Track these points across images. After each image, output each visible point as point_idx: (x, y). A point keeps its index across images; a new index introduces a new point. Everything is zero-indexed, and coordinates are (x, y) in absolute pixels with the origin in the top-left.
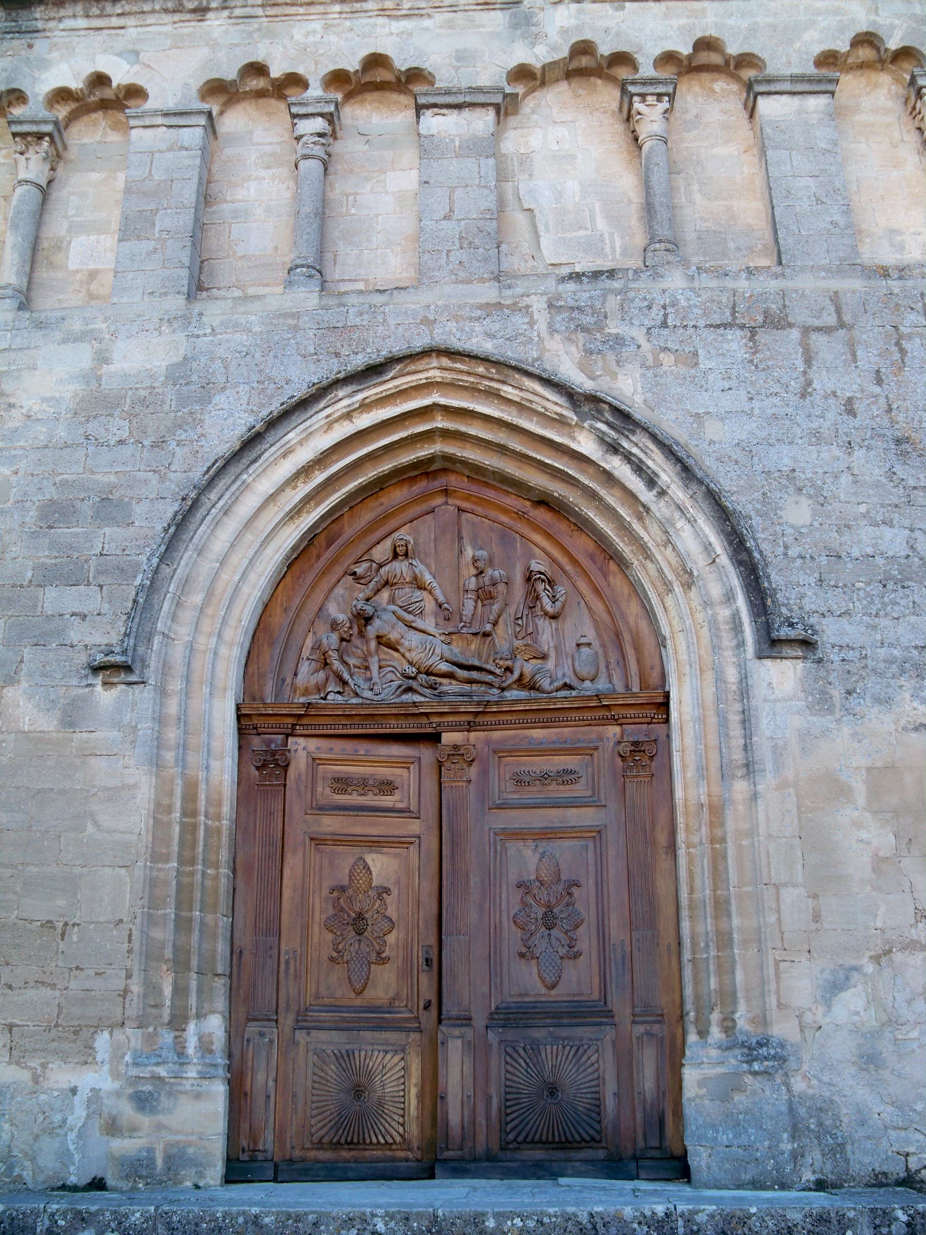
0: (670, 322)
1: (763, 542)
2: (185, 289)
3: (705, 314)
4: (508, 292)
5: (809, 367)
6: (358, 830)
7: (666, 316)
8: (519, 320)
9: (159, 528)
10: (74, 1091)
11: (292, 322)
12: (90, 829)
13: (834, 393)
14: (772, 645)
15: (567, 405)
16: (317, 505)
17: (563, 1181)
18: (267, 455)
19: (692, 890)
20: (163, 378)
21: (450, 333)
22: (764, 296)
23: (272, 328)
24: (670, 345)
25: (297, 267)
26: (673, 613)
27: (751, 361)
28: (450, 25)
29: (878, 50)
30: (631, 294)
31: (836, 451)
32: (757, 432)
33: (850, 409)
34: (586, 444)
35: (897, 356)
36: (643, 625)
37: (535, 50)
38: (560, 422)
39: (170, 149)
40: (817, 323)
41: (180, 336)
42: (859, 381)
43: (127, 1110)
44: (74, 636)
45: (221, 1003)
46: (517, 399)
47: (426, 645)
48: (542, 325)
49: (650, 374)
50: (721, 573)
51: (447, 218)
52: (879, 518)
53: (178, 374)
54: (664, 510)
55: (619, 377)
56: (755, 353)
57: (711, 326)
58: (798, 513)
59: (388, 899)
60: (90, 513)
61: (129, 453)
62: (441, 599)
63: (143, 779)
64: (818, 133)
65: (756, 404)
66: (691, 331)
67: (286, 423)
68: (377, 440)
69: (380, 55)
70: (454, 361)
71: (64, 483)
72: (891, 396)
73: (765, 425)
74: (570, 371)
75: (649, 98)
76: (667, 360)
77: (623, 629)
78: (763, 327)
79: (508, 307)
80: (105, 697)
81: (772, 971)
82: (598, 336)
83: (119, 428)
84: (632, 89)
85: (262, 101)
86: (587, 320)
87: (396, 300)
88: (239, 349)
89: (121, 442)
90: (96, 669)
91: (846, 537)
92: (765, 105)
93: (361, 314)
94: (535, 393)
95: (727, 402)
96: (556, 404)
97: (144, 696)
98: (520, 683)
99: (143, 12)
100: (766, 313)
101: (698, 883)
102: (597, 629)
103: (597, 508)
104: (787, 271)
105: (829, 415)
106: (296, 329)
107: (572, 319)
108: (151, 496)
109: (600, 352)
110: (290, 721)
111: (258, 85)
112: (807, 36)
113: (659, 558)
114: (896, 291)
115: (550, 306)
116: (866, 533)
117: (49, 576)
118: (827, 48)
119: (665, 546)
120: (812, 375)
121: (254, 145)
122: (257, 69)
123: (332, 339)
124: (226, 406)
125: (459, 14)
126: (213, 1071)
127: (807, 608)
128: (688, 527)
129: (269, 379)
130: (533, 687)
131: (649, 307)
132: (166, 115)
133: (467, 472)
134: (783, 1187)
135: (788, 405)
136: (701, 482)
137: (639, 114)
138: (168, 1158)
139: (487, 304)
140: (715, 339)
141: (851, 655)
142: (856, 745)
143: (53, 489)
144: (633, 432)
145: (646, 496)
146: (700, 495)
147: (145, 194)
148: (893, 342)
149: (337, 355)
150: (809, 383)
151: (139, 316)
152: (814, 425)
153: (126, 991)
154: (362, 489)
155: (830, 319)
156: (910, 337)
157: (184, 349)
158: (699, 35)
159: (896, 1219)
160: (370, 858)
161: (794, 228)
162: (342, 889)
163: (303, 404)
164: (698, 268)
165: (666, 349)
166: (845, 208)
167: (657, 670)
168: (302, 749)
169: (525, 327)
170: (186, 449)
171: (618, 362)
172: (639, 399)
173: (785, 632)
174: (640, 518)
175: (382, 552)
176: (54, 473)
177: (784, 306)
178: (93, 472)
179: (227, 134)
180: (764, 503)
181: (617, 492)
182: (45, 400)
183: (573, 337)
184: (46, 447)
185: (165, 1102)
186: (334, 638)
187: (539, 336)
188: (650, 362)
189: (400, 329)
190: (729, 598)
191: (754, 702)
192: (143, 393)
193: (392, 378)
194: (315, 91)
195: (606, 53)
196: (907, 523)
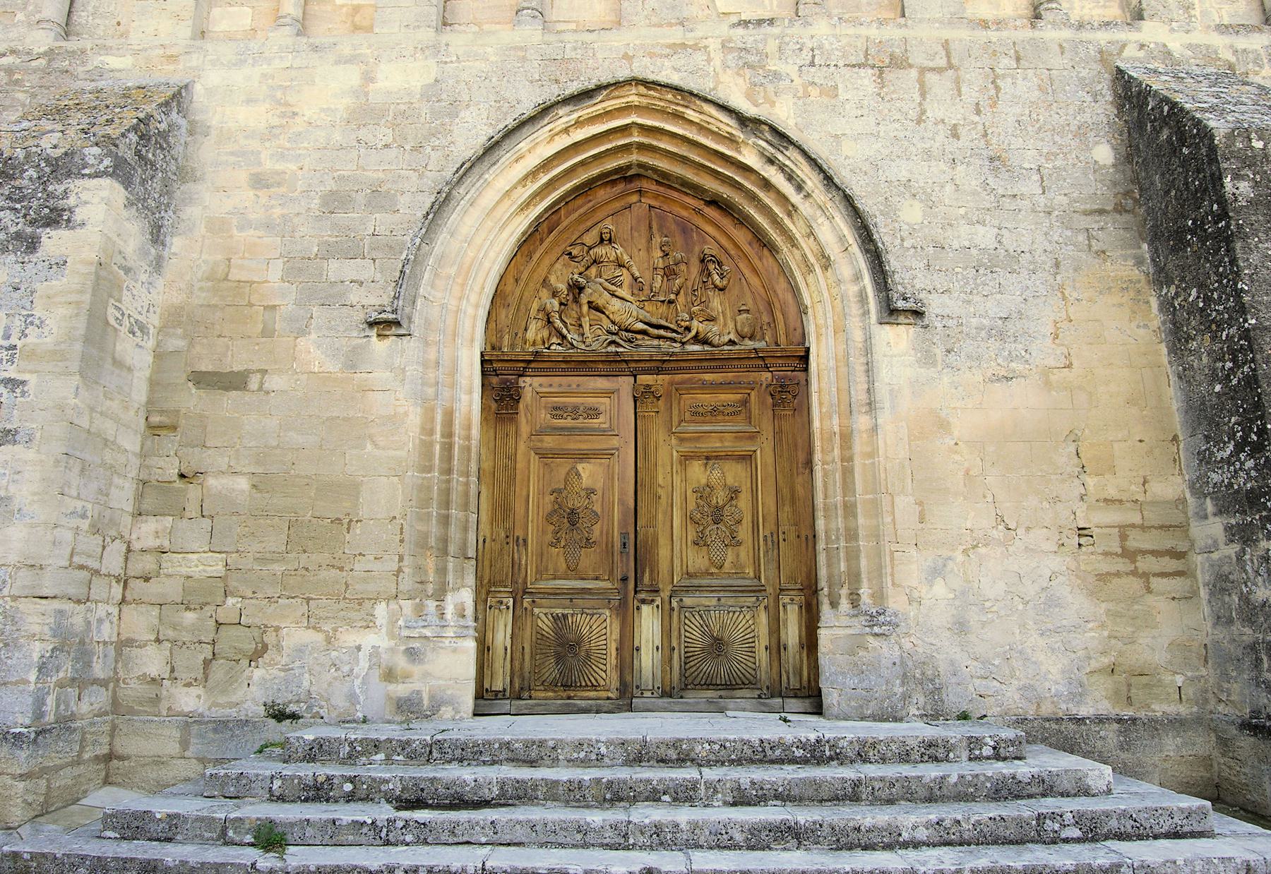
0: (817, 61)
1: (883, 234)
2: (434, 24)
4: (692, 35)
6: (572, 446)
7: (813, 56)
8: (699, 57)
9: (420, 214)
10: (359, 648)
11: (521, 54)
12: (369, 447)
13: (943, 120)
14: (891, 313)
16: (542, 200)
17: (729, 713)
18: (503, 159)
19: (826, 497)
21: (646, 67)
24: (816, 80)
25: (524, 9)
26: (813, 288)
30: (787, 39)
31: (942, 166)
34: (750, 158)
35: (993, 92)
36: (789, 297)
40: (931, 64)
41: (432, 62)
42: (962, 111)
43: (401, 662)
44: (353, 298)
45: (471, 579)
47: (624, 310)
48: (717, 62)
49: (800, 103)
50: (852, 259)
52: (975, 219)
53: (432, 91)
54: (809, 209)
58: (911, 213)
59: (594, 497)
60: (364, 202)
62: (637, 274)
63: (411, 409)
66: (832, 69)
67: (518, 134)
68: (587, 151)
70: (649, 89)
71: (341, 178)
76: (814, 92)
77: (775, 300)
80: (380, 346)
81: (888, 559)
82: (761, 71)
83: (384, 134)
86: (752, 59)
89: (386, 146)
90: (372, 324)
91: (949, 233)
98: (697, 339)
101: (830, 492)
102: (754, 299)
103: (756, 206)
104: (910, 22)
105: (938, 138)
106: (524, 59)
109: (762, 85)
110: (522, 365)
113: (804, 246)
114: (994, 40)
116: (964, 229)
117: (329, 252)
119: (808, 237)
120: (926, 105)
126: (465, 632)
127: (917, 287)
128: (827, 223)
130: (705, 342)
131: (801, 50)
133: (655, 177)
134: (896, 720)
136: (838, 188)
138: (432, 697)
141: (950, 323)
142: (953, 391)
143: (332, 182)
144: (787, 149)
145: (795, 198)
146: (837, 198)
149: (557, 81)
150: (923, 112)
152: (928, 146)
153: (400, 570)
154: (575, 189)
155: (942, 62)
156: (1004, 76)
157: (434, 72)
159: (986, 744)
160: (580, 467)
162: (559, 491)
163: (532, 119)
167: (799, 331)
168: (530, 385)
170: (439, 153)
172: (791, 122)
173: (900, 304)
174: (789, 215)
175: (590, 239)
176: (332, 170)
178: (364, 170)
180: (887, 206)
181: (772, 195)
182: (322, 110)
184: (325, 148)
185: (430, 655)
186: (556, 303)
190: (857, 277)
191: (875, 356)
192: (402, 107)
196: (996, 223)
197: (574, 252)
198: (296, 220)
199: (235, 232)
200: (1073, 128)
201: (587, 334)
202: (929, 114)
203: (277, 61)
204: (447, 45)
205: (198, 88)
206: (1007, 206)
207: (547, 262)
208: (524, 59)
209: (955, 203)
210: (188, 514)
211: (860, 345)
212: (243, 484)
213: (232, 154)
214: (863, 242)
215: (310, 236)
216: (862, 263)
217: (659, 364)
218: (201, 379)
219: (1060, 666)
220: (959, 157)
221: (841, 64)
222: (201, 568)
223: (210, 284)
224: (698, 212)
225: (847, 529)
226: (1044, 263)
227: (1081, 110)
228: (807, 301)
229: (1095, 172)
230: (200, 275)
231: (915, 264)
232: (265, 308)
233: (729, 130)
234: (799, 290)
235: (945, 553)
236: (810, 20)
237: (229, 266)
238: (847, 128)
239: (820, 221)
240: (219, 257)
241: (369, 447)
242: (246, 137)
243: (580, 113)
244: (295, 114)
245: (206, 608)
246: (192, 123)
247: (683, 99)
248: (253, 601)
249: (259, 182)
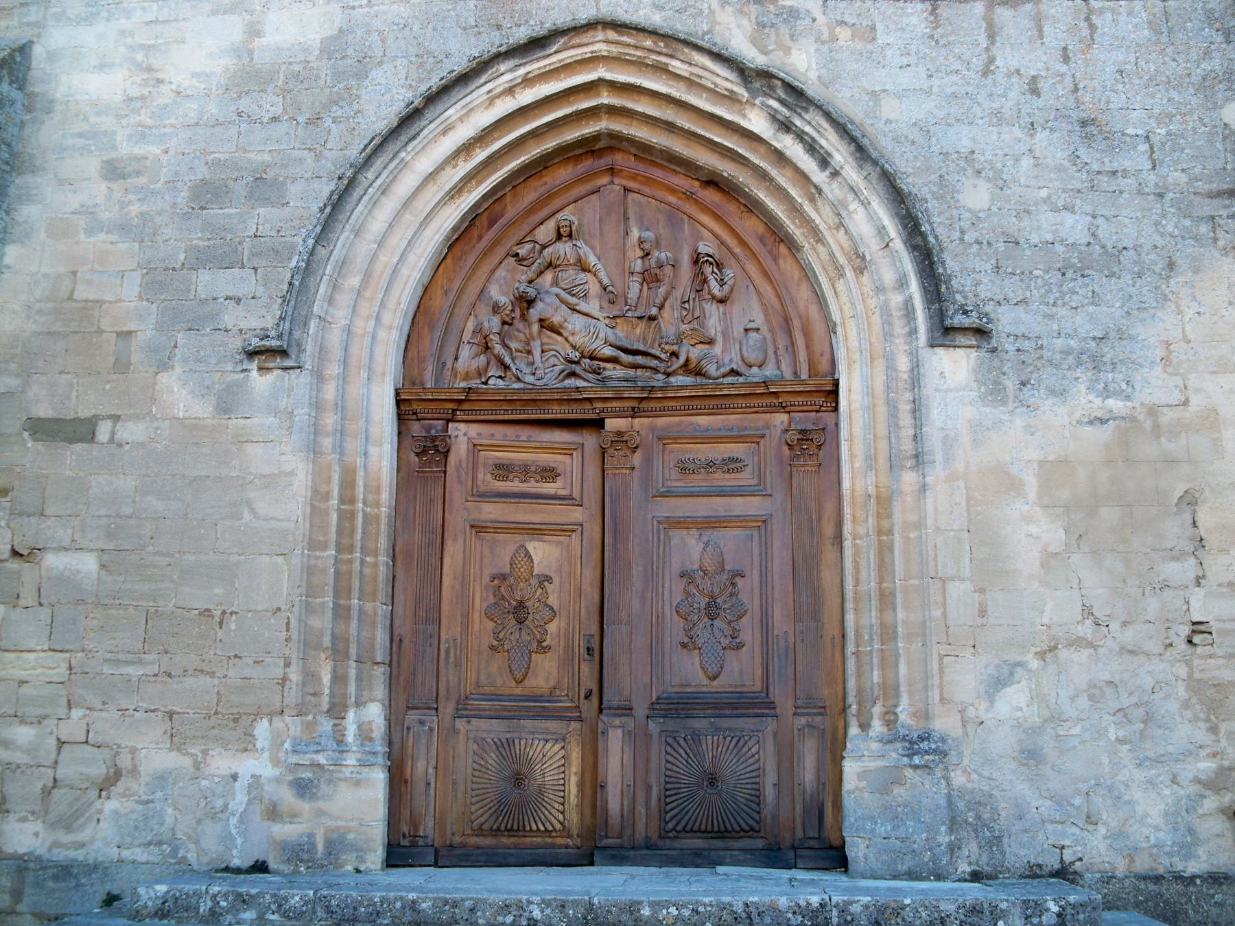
1: (938, 225)
5: (993, 43)
6: (520, 517)
9: (315, 208)
10: (235, 777)
12: (247, 516)
13: (1018, 72)
14: (945, 333)
15: (738, 80)
16: (479, 184)
18: (425, 132)
20: (317, 52)
24: (847, 18)
26: (844, 298)
27: (932, 37)
31: (1019, 133)
34: (757, 122)
35: (1086, 32)
36: (814, 311)
38: (730, 98)
42: (1044, 58)
43: (287, 797)
44: (228, 320)
46: (686, 74)
49: (825, 49)
52: (1061, 203)
53: (334, 47)
63: (301, 465)
65: (935, 81)
70: (621, 34)
71: (217, 162)
76: (844, 34)
81: (935, 665)
82: (772, 8)
83: (272, 104)
89: (275, 119)
90: (252, 354)
91: (1026, 223)
94: (705, 69)
95: (904, 80)
97: (300, 382)
98: (686, 368)
102: (766, 315)
103: (768, 188)
108: (306, 176)
109: (773, 25)
110: (451, 406)
113: (830, 240)
116: (1046, 218)
117: (201, 259)
119: (837, 228)
120: (995, 51)
123: (494, 11)
126: (372, 759)
127: (983, 296)
128: (861, 210)
129: (428, 52)
130: (699, 373)
133: (633, 150)
134: (939, 877)
136: (875, 163)
141: (1026, 345)
144: (806, 110)
145: (819, 176)
146: (874, 176)
148: (1083, 17)
149: (499, 27)
150: (992, 60)
152: (996, 105)
153: (285, 679)
156: (1101, 11)
160: (530, 546)
162: (503, 577)
163: (464, 79)
168: (462, 435)
170: (342, 126)
171: (792, 36)
172: (813, 75)
173: (958, 320)
174: (812, 200)
175: (545, 233)
176: (205, 152)
178: (246, 151)
180: (941, 186)
181: (789, 172)
183: (745, 9)
184: (197, 124)
185: (324, 788)
186: (496, 321)
187: (709, 8)
188: (825, 36)
190: (902, 283)
191: (924, 392)
192: (297, 68)
193: (556, 52)
197: (522, 251)
198: (158, 220)
199: (82, 237)
200: (1194, 79)
201: (538, 363)
203: (138, 13)
205: (38, 50)
206: (1104, 186)
207: (486, 268)
209: (1034, 183)
210: (22, 602)
211: (905, 376)
212: (88, 564)
213: (80, 135)
214: (910, 234)
215: (176, 241)
216: (908, 265)
217: (634, 404)
218: (42, 429)
219: (1162, 807)
220: (1039, 119)
222: (40, 671)
223: (50, 305)
224: (689, 196)
225: (883, 625)
226: (1154, 262)
227: (1207, 53)
228: (836, 317)
229: (1225, 138)
230: (38, 294)
231: (978, 264)
232: (119, 334)
233: (729, 86)
234: (825, 301)
235: (1015, 657)
237: (75, 282)
238: (890, 78)
239: (852, 207)
240: (62, 269)
241: (247, 516)
242: (98, 114)
244: (160, 82)
245: (46, 722)
246: (31, 96)
247: (666, 46)
248: (104, 714)
249: (113, 171)
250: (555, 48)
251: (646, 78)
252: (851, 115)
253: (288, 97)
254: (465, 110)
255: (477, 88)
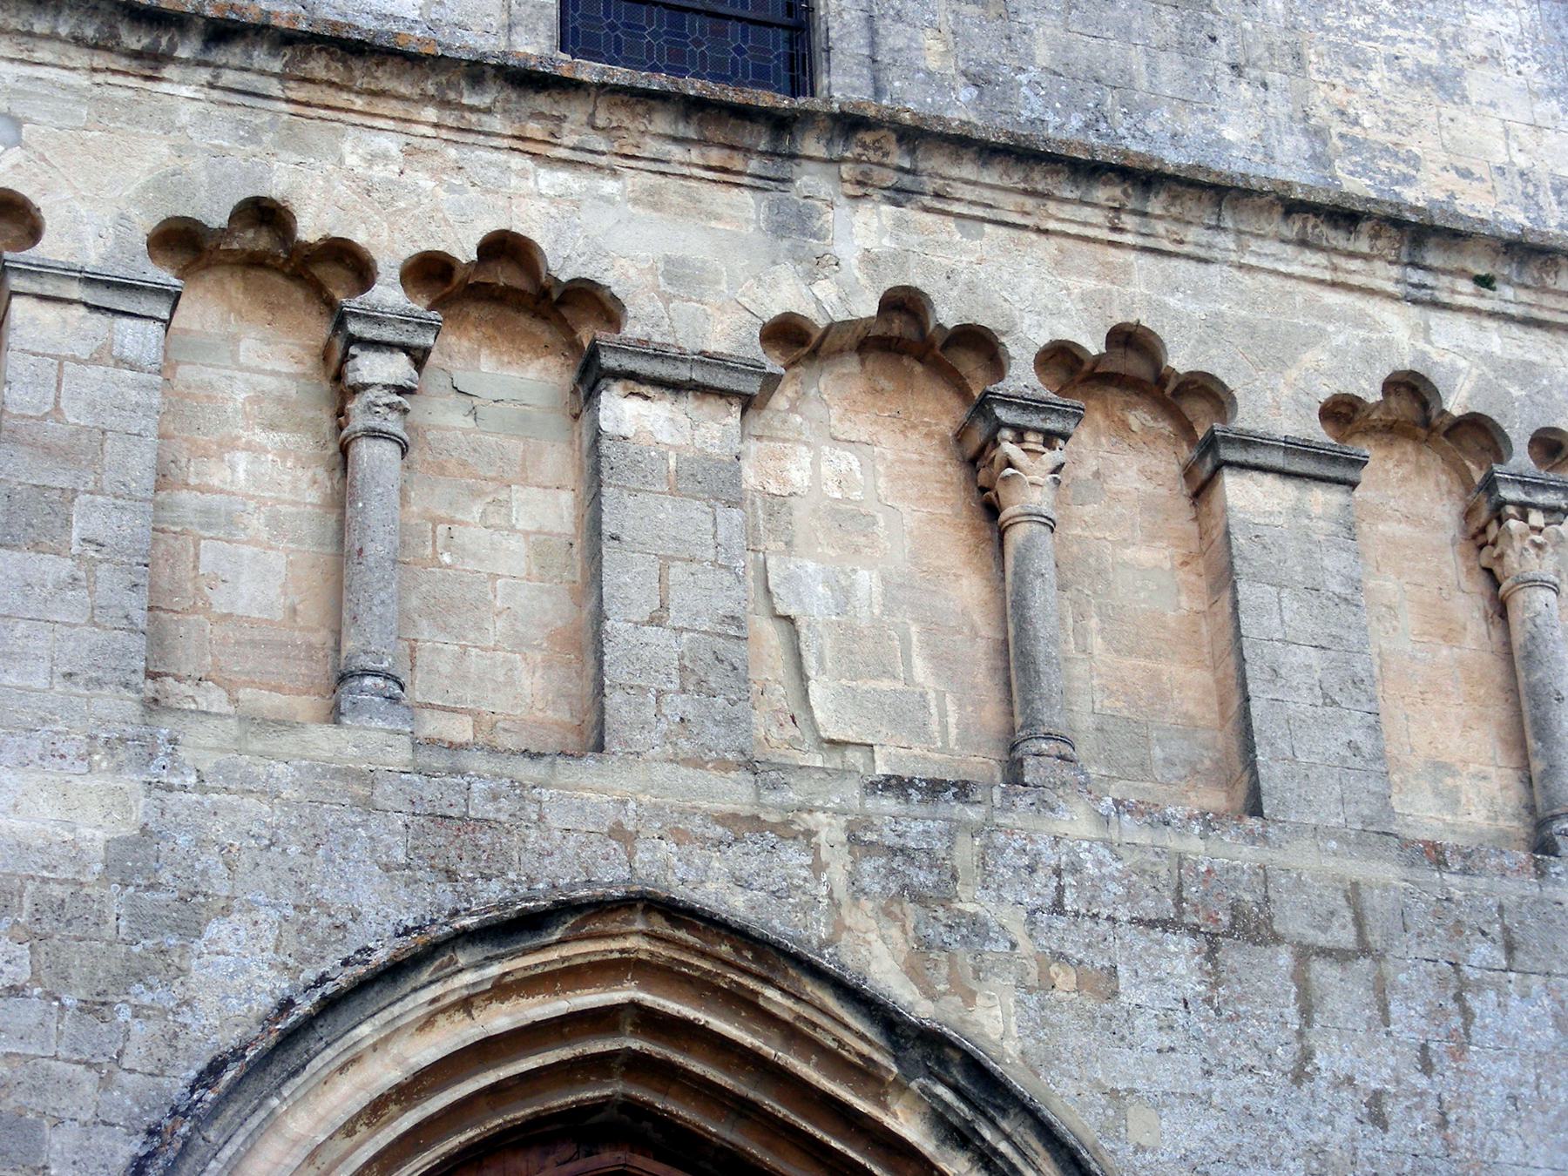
3: (1131, 896)
4: (771, 798)
5: (1308, 1023)
7: (1060, 890)
8: (794, 858)
11: (360, 790)
13: (1350, 1079)
15: (881, 1041)
18: (317, 1063)
20: (98, 867)
22: (1232, 875)
23: (321, 796)
24: (1069, 950)
27: (1209, 1001)
28: (653, 199)
29: (1425, 405)
32: (1218, 1139)
33: (1376, 1116)
34: (908, 1125)
35: (1456, 1022)
37: (815, 289)
38: (864, 1074)
39: (94, 360)
40: (1323, 940)
42: (1392, 1060)
46: (787, 1017)
48: (837, 874)
49: (1032, 1001)
51: (655, 620)
53: (132, 859)
55: (980, 1000)
56: (1214, 986)
57: (1140, 921)
61: (33, 1019)
64: (1327, 562)
65: (1216, 1083)
69: (516, 236)
72: (1446, 1096)
73: (1232, 1126)
74: (886, 975)
75: (1030, 437)
78: (1229, 935)
79: (773, 828)
82: (941, 913)
84: (1002, 413)
85: (253, 274)
86: (922, 878)
87: (562, 780)
88: (255, 830)
92: (1236, 490)
93: (495, 798)
94: (824, 1011)
95: (1165, 1075)
96: (862, 1037)
99: (30, 34)
100: (1235, 909)
104: (1272, 831)
107: (893, 871)
108: (83, 1117)
111: (263, 251)
112: (1309, 358)
114: (1458, 895)
115: (853, 839)
118: (1343, 391)
120: (1313, 1040)
121: (242, 368)
122: (265, 214)
123: (442, 841)
124: (231, 946)
125: (669, 180)
129: (319, 904)
131: (1032, 869)
132: (90, 281)
135: (1271, 1093)
137: (1010, 464)
139: (735, 816)
140: (1145, 949)
144: (1004, 1112)
147: (48, 450)
148: (1451, 993)
149: (451, 875)
150: (1307, 1055)
151: (44, 721)
152: (1317, 1137)
156: (1479, 986)
157: (141, 809)
158: (1119, 319)
161: (1283, 745)
163: (396, 971)
164: (1117, 803)
165: (1060, 957)
166: (1371, 719)
169: (804, 873)
171: (977, 971)
177: (1267, 899)
179: (186, 331)
183: (896, 909)
187: (830, 895)
188: (1032, 979)
189: (572, 837)
192: (57, 891)
193: (560, 942)
194: (388, 293)
195: (950, 324)
202: (1320, 1060)
204: (173, 741)
208: (367, 806)
221: (1123, 914)
233: (865, 1049)
236: (1050, 796)
243: (507, 966)
247: (758, 958)
250: (555, 938)
251: (718, 1016)
252: (1078, 1130)
253: (43, 948)
254: (388, 1031)
255: (415, 990)
